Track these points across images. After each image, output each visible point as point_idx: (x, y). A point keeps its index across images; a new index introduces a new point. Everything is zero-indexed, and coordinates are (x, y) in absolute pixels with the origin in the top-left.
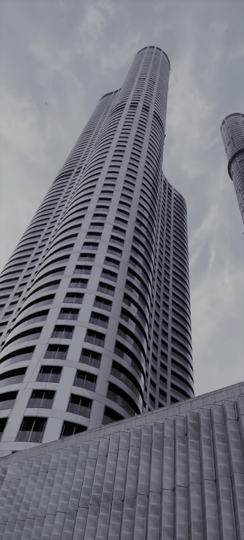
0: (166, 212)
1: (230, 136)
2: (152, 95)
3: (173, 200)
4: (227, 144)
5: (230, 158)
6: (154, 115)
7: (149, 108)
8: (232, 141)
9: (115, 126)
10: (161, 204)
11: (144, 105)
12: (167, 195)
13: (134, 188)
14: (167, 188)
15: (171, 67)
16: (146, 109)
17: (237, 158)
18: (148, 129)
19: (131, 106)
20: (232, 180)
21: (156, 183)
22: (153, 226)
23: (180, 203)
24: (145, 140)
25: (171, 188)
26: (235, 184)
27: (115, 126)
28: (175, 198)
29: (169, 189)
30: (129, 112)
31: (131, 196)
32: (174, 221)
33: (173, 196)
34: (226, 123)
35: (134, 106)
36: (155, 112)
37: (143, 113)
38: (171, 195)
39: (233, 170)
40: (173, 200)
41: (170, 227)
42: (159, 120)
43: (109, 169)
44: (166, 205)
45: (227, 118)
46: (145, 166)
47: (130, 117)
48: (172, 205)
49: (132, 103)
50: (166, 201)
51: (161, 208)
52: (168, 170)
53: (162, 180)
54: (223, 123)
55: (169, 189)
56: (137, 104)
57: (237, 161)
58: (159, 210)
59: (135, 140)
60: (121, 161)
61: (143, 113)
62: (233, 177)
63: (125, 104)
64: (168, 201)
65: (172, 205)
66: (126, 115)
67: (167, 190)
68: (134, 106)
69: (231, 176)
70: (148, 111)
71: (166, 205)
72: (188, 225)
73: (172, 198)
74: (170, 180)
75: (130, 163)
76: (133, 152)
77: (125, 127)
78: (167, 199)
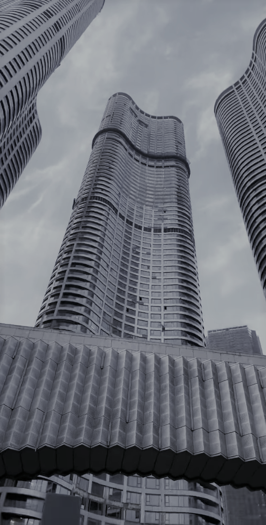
0: (17, 134)
1: (113, 111)
2: (70, 19)
3: (31, 128)
4: (106, 115)
5: (102, 129)
6: (61, 39)
7: (61, 28)
8: (112, 116)
9: (19, 18)
10: (18, 123)
11: (57, 22)
12: (28, 119)
13: (10, 80)
14: (32, 112)
15: (102, 10)
16: (57, 27)
17: (107, 133)
18: (43, 51)
19: (44, 12)
20: (92, 148)
21: (24, 97)
22: (27, 100)
23: (36, 135)
24: (8, 84)
25: (35, 115)
26: (93, 153)
27: (19, 18)
28: (33, 127)
29: (33, 115)
30: (12, 35)
31: (29, 60)
32: (20, 147)
33: (33, 123)
34: (117, 98)
35: (48, 14)
36: (63, 36)
37: (52, 28)
38: (31, 122)
39: (99, 140)
40: (31, 128)
41: (13, 149)
42: (62, 47)
43: (5, 38)
44: (16, 135)
45: (120, 94)
46: (24, 78)
47: (37, 22)
48: (28, 132)
49: (47, 11)
50: (16, 135)
51: (14, 127)
52: (44, 98)
53: (31, 102)
54: (115, 95)
55: (33, 115)
56: (52, 15)
57: (106, 136)
58: (11, 127)
59: (33, 43)
60: (7, 50)
61: (52, 28)
62: (94, 147)
63: (40, 6)
64: (21, 132)
65: (28, 132)
66: (22, 25)
67: (31, 114)
68: (48, 14)
69: (93, 145)
70: (58, 30)
71: (10, 144)
72: (17, 184)
73: (31, 126)
74: (39, 107)
75: (10, 63)
76: (7, 65)
77: (23, 29)
78: (26, 122)
